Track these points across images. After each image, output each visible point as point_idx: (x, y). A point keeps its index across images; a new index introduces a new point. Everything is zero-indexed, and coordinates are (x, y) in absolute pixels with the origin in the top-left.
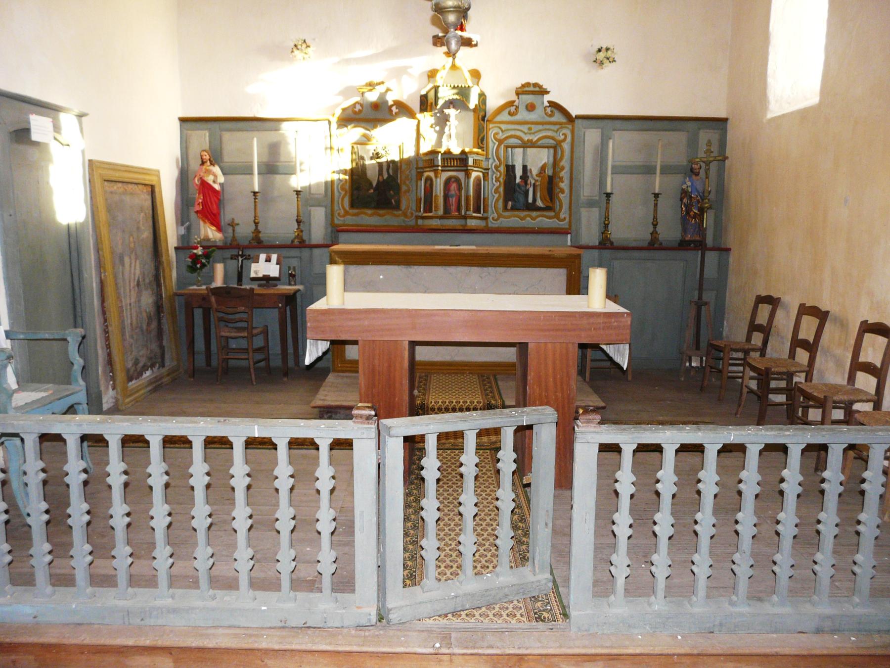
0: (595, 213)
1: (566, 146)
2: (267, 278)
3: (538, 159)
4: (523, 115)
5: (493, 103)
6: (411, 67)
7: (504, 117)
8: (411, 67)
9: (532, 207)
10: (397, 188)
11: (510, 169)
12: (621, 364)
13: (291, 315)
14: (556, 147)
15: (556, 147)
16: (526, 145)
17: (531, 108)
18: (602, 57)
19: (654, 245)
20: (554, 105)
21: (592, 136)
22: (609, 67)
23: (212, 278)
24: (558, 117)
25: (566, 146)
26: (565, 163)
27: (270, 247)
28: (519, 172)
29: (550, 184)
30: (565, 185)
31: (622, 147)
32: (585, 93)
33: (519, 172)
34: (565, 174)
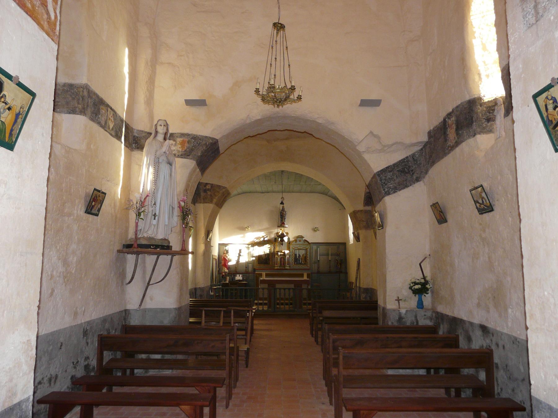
0: (316, 265)
1: (309, 250)
2: (239, 280)
3: (302, 252)
4: (298, 242)
5: (292, 239)
6: (257, 91)
7: (294, 243)
8: (257, 91)
9: (301, 264)
10: (269, 259)
11: (296, 255)
12: (121, 116)
13: (176, 361)
14: (306, 250)
15: (306, 250)
16: (299, 249)
17: (300, 241)
18: (315, 230)
19: (330, 272)
20: (306, 241)
21: (315, 247)
22: (318, 232)
23: (226, 281)
24: (306, 243)
25: (309, 250)
26: (308, 253)
27: (239, 274)
28: (298, 256)
29: (305, 258)
30: (308, 259)
31: (321, 249)
32: (312, 237)
33: (298, 256)
34: (308, 256)
